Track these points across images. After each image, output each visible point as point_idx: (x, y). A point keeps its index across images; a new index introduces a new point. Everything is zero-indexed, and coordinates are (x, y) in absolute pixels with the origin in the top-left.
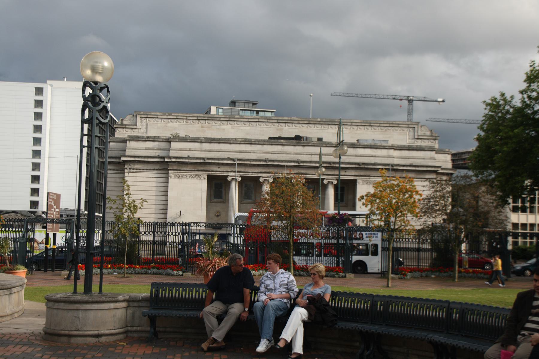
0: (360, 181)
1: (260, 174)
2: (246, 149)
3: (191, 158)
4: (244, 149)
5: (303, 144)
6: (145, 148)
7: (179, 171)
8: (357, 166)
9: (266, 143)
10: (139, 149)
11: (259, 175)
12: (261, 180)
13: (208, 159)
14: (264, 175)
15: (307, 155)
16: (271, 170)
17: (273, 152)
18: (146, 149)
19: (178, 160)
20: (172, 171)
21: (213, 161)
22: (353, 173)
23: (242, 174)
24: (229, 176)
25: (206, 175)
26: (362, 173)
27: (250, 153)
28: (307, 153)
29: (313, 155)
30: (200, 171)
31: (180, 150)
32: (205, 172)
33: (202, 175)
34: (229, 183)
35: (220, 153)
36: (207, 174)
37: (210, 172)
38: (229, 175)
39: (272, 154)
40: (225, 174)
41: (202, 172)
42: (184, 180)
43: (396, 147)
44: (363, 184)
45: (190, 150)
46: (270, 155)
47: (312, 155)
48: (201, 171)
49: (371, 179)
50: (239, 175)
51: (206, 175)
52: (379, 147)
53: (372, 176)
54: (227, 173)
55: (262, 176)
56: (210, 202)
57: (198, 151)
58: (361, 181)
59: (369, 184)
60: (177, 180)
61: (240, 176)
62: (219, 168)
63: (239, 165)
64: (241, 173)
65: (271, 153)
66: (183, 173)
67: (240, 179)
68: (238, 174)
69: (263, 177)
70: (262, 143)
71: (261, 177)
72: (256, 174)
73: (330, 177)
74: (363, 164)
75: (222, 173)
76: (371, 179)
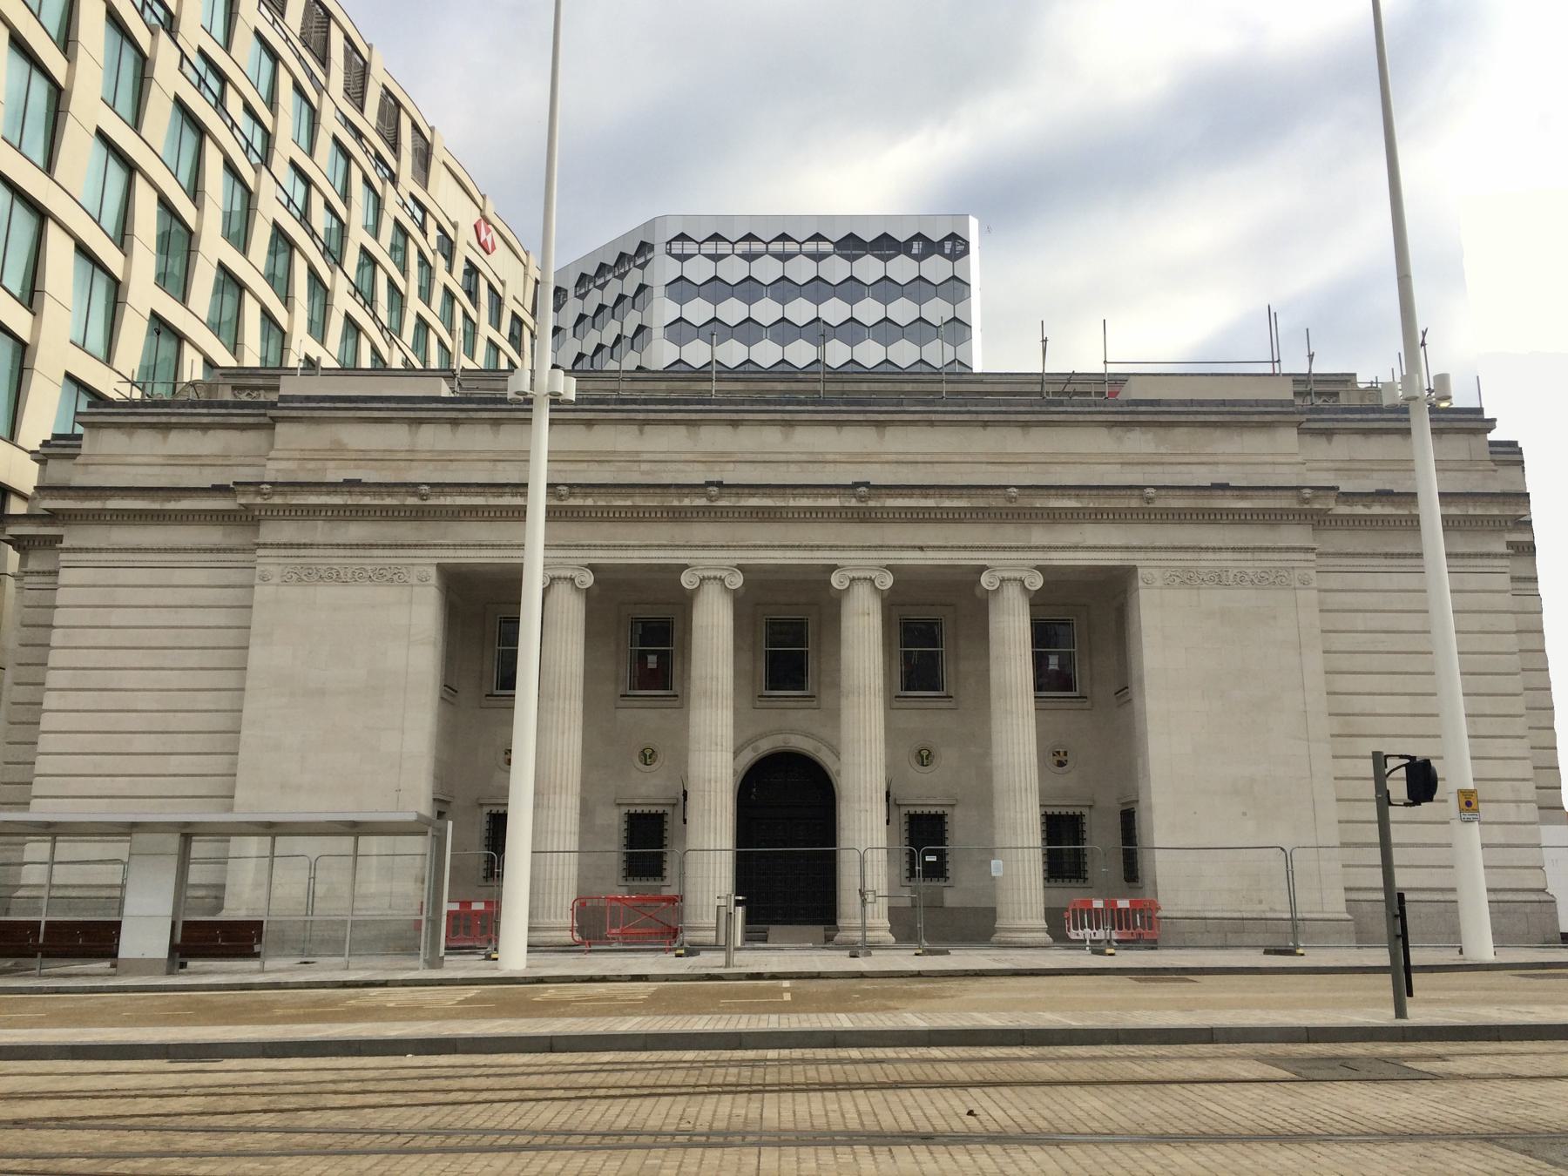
42: (326, 593)
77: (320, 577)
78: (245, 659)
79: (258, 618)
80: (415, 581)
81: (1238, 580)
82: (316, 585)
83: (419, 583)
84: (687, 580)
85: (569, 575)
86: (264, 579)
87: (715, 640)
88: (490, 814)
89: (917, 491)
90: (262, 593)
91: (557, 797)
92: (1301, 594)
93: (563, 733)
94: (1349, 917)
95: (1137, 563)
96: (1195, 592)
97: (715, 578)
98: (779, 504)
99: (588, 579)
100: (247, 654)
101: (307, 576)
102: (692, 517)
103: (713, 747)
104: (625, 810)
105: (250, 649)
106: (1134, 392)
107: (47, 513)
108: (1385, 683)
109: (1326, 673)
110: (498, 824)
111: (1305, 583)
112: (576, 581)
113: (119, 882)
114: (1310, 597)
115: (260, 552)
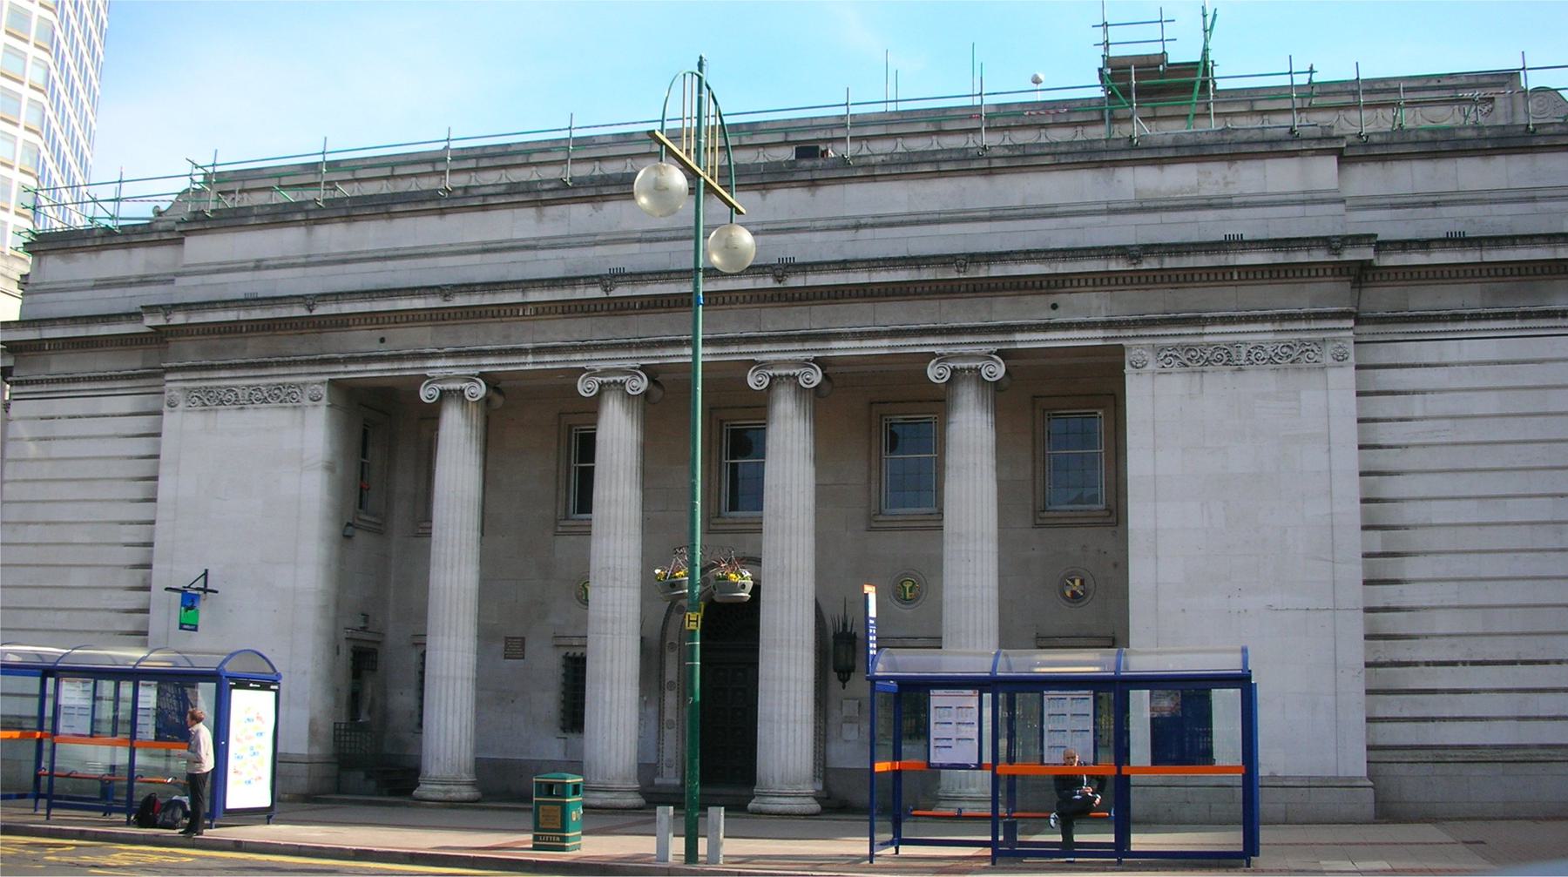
0: (1138, 347)
1: (578, 357)
2: (518, 235)
3: (1469, 239)
4: (507, 236)
5: (807, 176)
6: (92, 283)
7: (205, 375)
8: (1115, 265)
9: (613, 190)
10: (70, 290)
11: (577, 359)
12: (426, 394)
13: (324, 297)
14: (437, 368)
15: (828, 229)
16: (469, 336)
17: (649, 236)
18: (94, 287)
19: (196, 318)
20: (179, 376)
21: (347, 308)
22: (1097, 305)
23: (490, 364)
24: (426, 377)
25: (322, 383)
26: (1155, 302)
27: (534, 248)
28: (834, 223)
29: (865, 226)
30: (295, 363)
31: (218, 272)
32: (317, 369)
33: (305, 384)
34: (432, 415)
35: (390, 264)
36: (326, 378)
37: (342, 368)
38: (428, 373)
39: (646, 246)
40: (409, 368)
41: (305, 369)
42: (228, 418)
43: (884, 165)
44: (187, 410)
45: (259, 266)
46: (635, 248)
47: (857, 227)
48: (302, 363)
49: (1207, 339)
50: (476, 371)
51: (322, 383)
52: (1244, 149)
53: (1214, 321)
54: (418, 364)
55: (592, 365)
56: (870, 529)
57: (293, 265)
58: (1149, 356)
59: (1197, 367)
60: (1176, 384)
61: (482, 375)
62: (382, 340)
63: (545, 310)
64: (485, 361)
65: (639, 241)
66: (222, 380)
67: (999, 370)
68: (470, 366)
69: (593, 373)
70: (592, 192)
71: (583, 370)
72: (558, 358)
73: (965, 345)
74: (1149, 249)
75: (396, 365)
76: (1207, 339)
77: (222, 401)
78: (155, 490)
79: (167, 445)
80: (1328, 360)
81: (1252, 358)
82: (217, 410)
83: (1336, 362)
84: (585, 387)
85: (458, 387)
86: (172, 405)
87: (615, 456)
88: (566, 657)
89: (48, 323)
90: (170, 420)
91: (446, 638)
92: (1333, 374)
93: (452, 567)
94: (1371, 783)
95: (1125, 343)
96: (1197, 376)
97: (788, 376)
98: (925, 277)
99: (480, 390)
100: (157, 486)
101: (211, 400)
102: (1309, 276)
103: (610, 583)
104: (563, 651)
105: (160, 479)
106: (681, 167)
107: (150, 330)
108: (1445, 485)
109: (1362, 474)
110: (575, 670)
111: (1340, 359)
112: (466, 392)
113: (1045, 762)
114: (1344, 378)
115: (169, 377)
